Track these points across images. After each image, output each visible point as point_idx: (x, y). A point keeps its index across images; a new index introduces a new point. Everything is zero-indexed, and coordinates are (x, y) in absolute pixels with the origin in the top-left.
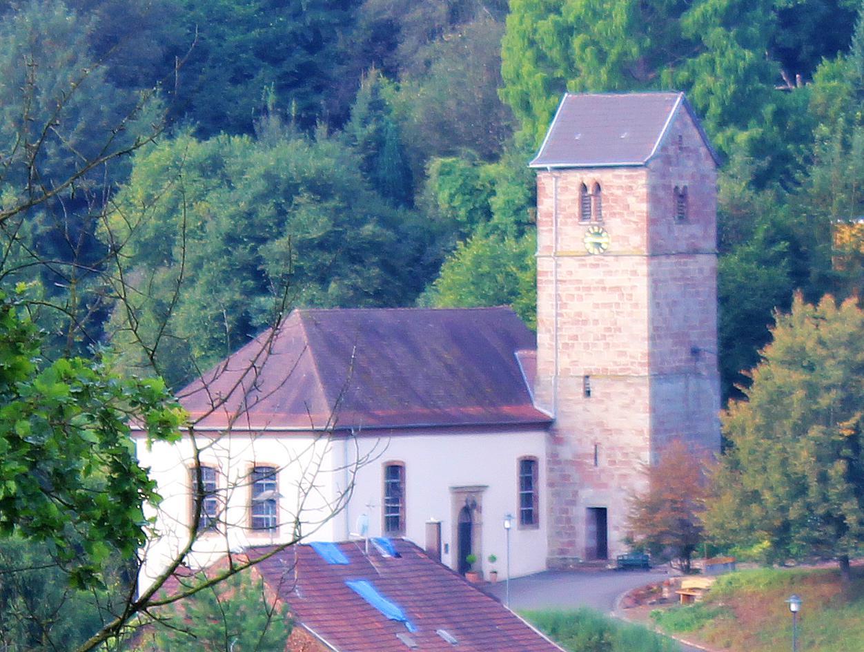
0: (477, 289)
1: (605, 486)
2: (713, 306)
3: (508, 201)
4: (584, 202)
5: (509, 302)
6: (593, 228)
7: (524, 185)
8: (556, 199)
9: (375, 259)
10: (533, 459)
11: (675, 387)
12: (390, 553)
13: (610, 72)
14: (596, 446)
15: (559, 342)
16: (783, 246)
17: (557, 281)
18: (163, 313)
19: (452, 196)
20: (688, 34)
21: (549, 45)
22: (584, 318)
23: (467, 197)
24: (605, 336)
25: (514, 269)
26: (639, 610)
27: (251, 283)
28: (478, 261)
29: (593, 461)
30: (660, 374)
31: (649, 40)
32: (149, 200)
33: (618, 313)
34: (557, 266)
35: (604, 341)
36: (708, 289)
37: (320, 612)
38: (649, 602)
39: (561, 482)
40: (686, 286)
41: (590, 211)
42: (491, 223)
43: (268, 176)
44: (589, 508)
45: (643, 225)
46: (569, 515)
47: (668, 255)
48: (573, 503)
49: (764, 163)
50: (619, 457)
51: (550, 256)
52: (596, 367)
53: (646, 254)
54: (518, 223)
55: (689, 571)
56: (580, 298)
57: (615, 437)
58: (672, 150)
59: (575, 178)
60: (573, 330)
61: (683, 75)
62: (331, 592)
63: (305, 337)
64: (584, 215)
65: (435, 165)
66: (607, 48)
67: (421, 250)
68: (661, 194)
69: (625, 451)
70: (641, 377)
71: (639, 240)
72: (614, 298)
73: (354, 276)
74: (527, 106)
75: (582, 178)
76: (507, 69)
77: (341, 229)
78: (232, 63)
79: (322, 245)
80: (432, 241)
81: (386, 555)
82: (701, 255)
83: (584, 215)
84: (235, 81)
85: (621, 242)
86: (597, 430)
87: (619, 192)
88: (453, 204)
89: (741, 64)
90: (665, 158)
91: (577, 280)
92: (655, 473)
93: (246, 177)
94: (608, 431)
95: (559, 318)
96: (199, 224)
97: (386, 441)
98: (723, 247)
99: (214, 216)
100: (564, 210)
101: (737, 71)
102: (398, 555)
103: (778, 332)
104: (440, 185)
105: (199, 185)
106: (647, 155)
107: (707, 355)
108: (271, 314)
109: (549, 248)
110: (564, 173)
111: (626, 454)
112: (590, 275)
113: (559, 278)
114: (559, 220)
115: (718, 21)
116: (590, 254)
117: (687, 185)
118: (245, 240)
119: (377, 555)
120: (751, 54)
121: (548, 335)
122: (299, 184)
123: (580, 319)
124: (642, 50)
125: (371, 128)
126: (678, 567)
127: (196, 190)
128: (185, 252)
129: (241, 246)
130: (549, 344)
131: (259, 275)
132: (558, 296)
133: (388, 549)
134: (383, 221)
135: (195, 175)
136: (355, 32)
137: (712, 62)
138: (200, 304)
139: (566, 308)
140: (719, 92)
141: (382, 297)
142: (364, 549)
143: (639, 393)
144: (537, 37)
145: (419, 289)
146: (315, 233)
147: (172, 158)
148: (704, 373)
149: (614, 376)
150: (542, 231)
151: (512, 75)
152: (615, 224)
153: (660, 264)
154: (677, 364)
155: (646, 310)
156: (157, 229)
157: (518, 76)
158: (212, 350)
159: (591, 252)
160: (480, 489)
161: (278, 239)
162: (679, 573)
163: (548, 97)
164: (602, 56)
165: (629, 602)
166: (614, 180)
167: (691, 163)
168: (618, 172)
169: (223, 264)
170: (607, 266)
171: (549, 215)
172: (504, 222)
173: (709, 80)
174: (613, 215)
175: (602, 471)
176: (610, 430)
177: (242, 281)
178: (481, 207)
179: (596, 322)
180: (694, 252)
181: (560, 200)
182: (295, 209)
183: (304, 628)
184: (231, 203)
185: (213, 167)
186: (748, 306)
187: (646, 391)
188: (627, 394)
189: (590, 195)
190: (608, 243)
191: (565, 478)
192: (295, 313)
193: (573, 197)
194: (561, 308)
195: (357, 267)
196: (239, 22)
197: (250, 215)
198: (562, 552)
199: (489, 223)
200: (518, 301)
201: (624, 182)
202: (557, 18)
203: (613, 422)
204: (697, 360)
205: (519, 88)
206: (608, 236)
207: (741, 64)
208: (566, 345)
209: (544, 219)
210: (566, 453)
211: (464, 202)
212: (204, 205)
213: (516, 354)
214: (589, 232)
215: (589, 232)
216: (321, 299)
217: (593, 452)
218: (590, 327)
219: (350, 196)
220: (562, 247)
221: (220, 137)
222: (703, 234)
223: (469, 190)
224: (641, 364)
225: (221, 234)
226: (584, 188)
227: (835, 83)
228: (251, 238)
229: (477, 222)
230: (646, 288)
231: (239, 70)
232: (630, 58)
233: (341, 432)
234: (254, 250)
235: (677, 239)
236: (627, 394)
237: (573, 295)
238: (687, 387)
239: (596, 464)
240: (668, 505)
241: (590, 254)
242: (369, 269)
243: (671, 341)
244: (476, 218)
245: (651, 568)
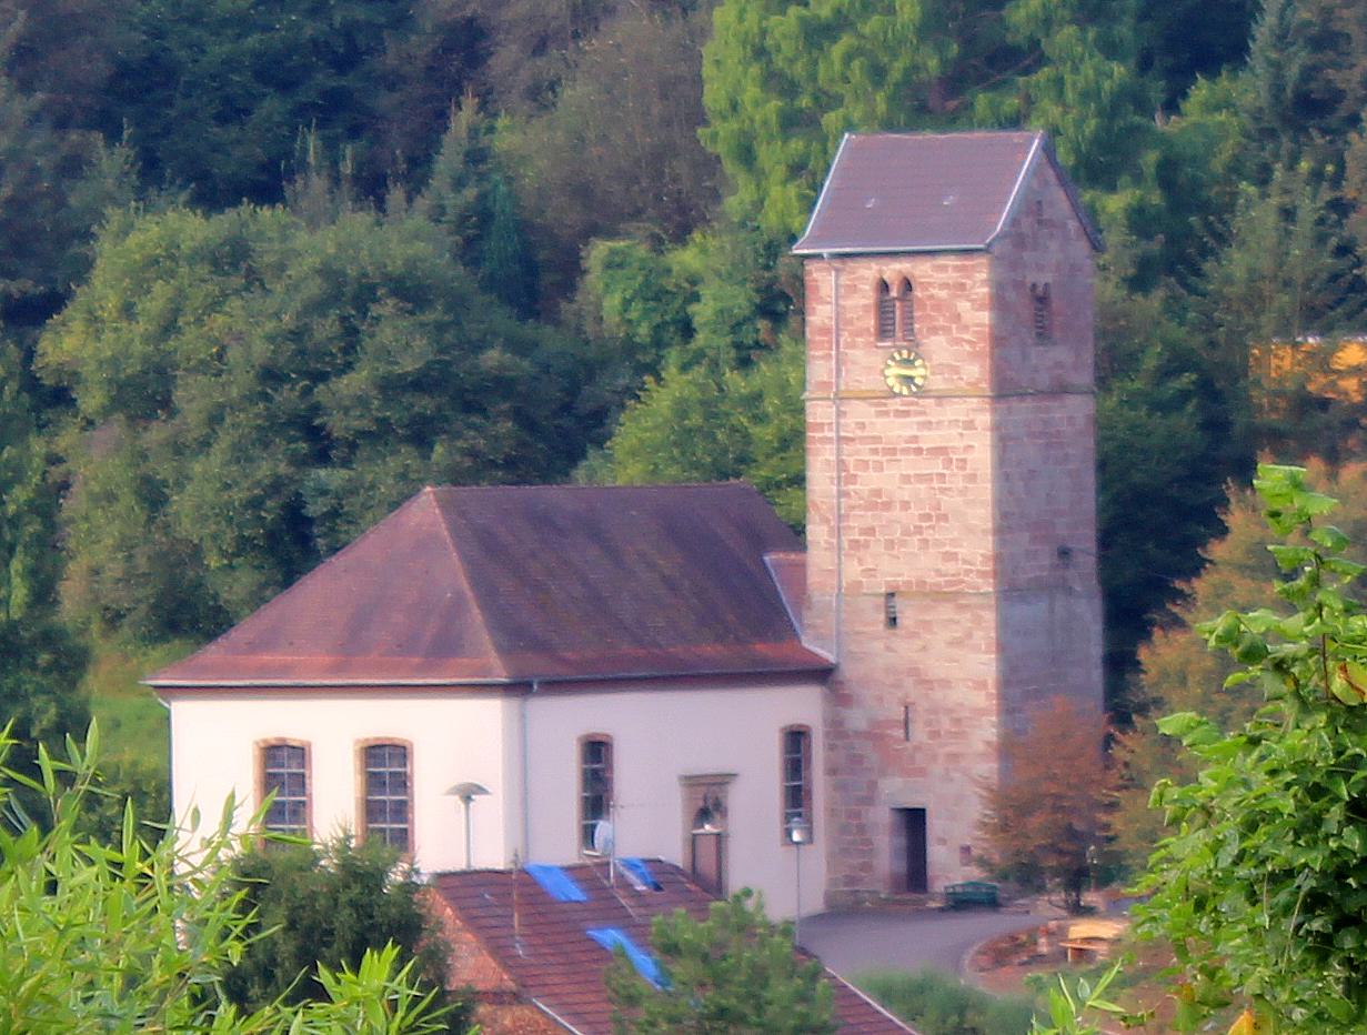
0: (683, 453)
1: (922, 772)
2: (1090, 479)
3: (722, 311)
4: (883, 310)
5: (738, 475)
6: (900, 354)
7: (748, 285)
8: (837, 305)
9: (505, 406)
10: (802, 729)
11: (1037, 610)
12: (646, 884)
13: (891, 99)
14: (906, 707)
15: (843, 538)
16: (1187, 379)
17: (840, 439)
18: (153, 496)
19: (627, 303)
20: (1017, 38)
21: (790, 55)
22: (884, 499)
23: (652, 304)
24: (921, 527)
25: (744, 420)
26: (1004, 973)
27: (303, 447)
28: (681, 410)
29: (902, 731)
30: (1012, 589)
31: (955, 46)
32: (128, 311)
33: (943, 491)
34: (840, 414)
35: (919, 537)
36: (1081, 454)
37: (556, 980)
38: (1017, 961)
39: (847, 767)
40: (1048, 446)
41: (894, 324)
42: (693, 346)
43: (326, 272)
44: (893, 809)
45: (984, 346)
46: (864, 821)
47: (1022, 396)
48: (869, 800)
49: (1155, 246)
50: (945, 724)
51: (829, 399)
52: (905, 578)
53: (990, 394)
54: (738, 346)
55: (1080, 911)
56: (879, 467)
57: (938, 694)
58: (1026, 225)
59: (869, 272)
60: (869, 519)
61: (1011, 103)
62: (568, 948)
63: (446, 533)
64: (884, 331)
65: (597, 252)
66: (886, 60)
67: (573, 391)
68: (1011, 296)
69: (955, 715)
70: (982, 594)
71: (976, 371)
72: (937, 466)
73: (472, 433)
74: (746, 156)
75: (880, 271)
76: (714, 96)
77: (447, 358)
78: (217, 89)
79: (420, 383)
80: (590, 377)
81: (641, 888)
82: (1071, 396)
83: (885, 331)
84: (222, 119)
85: (946, 376)
86: (909, 682)
87: (943, 294)
88: (627, 316)
89: (1107, 85)
90: (1017, 238)
91: (873, 437)
92: (1007, 749)
93: (288, 273)
94: (926, 683)
95: (842, 500)
96: (214, 350)
98: (1103, 383)
99: (239, 337)
100: (850, 322)
101: (1100, 97)
102: (658, 888)
103: (1236, 518)
104: (607, 285)
105: (210, 287)
106: (989, 233)
107: (1081, 559)
108: (337, 497)
109: (825, 385)
110: (851, 264)
111: (958, 721)
112: (897, 430)
113: (843, 434)
114: (842, 340)
115: (1067, 13)
116: (895, 395)
117: (1050, 281)
118: (293, 376)
119: (628, 886)
120: (1122, 69)
121: (826, 528)
122: (378, 284)
123: (879, 501)
124: (943, 62)
125: (470, 193)
126: (1062, 904)
127: (207, 296)
128: (193, 398)
129: (288, 387)
130: (826, 542)
131: (315, 433)
132: (841, 464)
133: (642, 876)
134: (521, 347)
135: (203, 270)
136: (414, 38)
137: (1059, 82)
138: (220, 481)
139: (855, 483)
140: (1071, 131)
141: (517, 468)
142: (608, 877)
143: (978, 620)
144: (769, 42)
145: (574, 456)
146: (409, 365)
147: (164, 244)
148: (1078, 588)
149: (938, 593)
150: (813, 357)
151: (723, 104)
152: (938, 347)
153: (1009, 409)
154: (1038, 573)
155: (989, 486)
156: (145, 359)
157: (735, 106)
158: (239, 556)
159: (896, 390)
160: (722, 780)
161: (346, 373)
162: (1064, 913)
163: (785, 141)
164: (878, 74)
165: (984, 961)
166: (935, 274)
167: (1054, 245)
168: (941, 261)
169: (257, 416)
170: (924, 413)
171: (825, 331)
172: (715, 345)
173: (1055, 111)
174: (934, 330)
175: (917, 748)
176: (927, 681)
177: (289, 443)
178: (675, 322)
179: (905, 505)
180: (1060, 390)
181: (844, 307)
182: (371, 325)
183: (538, 1008)
184: (270, 317)
185: (233, 259)
186: (1137, 477)
187: (990, 617)
188: (958, 622)
189: (894, 299)
190: (924, 377)
191: (856, 760)
192: (425, 494)
194: (846, 484)
195: (476, 419)
196: (225, 22)
197: (296, 335)
198: (851, 880)
199: (688, 347)
200: (752, 472)
201: (951, 276)
202: (803, 12)
203: (936, 667)
204: (1067, 566)
205: (735, 126)
206: (925, 367)
207: (1107, 85)
208: (855, 544)
209: (818, 338)
210: (856, 719)
211: (646, 313)
212: (220, 319)
213: (767, 558)
214: (893, 359)
215: (893, 359)
216: (419, 472)
217: (903, 717)
218: (897, 513)
219: (457, 303)
220: (847, 384)
221: (242, 208)
222: (1073, 359)
223: (654, 294)
224: (982, 574)
225: (253, 366)
226: (884, 287)
227: (1222, 117)
228: (304, 374)
229: (669, 345)
230: (989, 449)
231: (227, 100)
232: (923, 75)
233: (518, 688)
234: (307, 392)
235: (1036, 370)
236: (958, 622)
237: (867, 462)
238: (1052, 611)
239: (907, 738)
240: (1049, 802)
241: (895, 395)
242: (495, 423)
243: (1026, 536)
244: (666, 337)
245: (1001, 905)
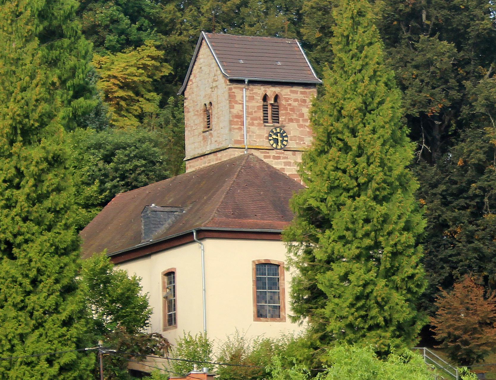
97: (154, 258)
168: (295, 89)
170: (287, 158)
174: (291, 120)
193: (258, 104)
201: (300, 96)
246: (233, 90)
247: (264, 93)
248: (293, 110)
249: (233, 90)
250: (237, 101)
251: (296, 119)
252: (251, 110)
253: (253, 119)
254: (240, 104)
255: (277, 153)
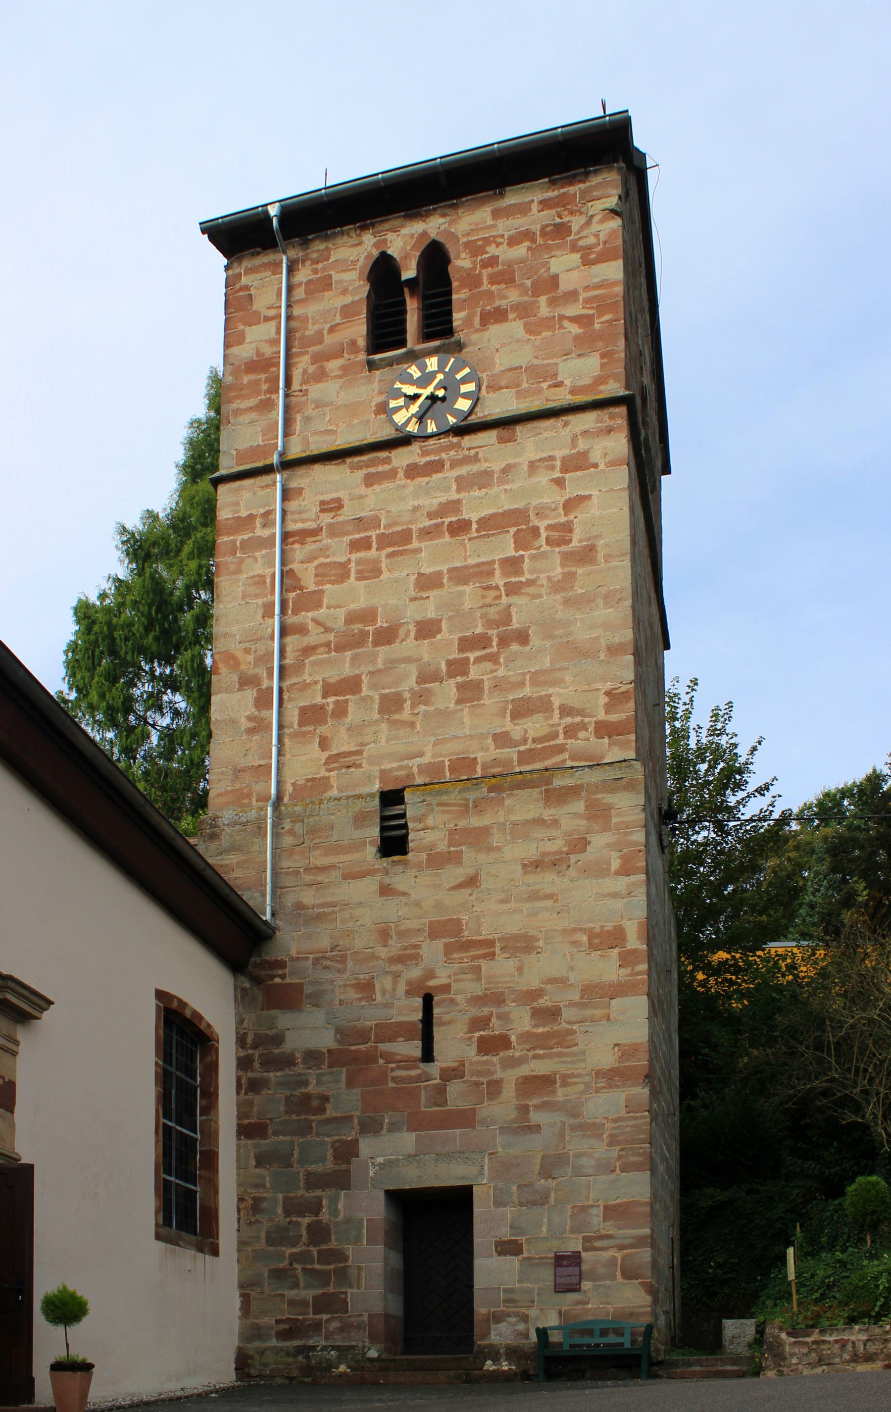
246: (244, 280)
247: (376, 253)
248: (506, 277)
249: (244, 280)
250: (258, 313)
251: (516, 307)
252: (317, 327)
253: (318, 358)
254: (267, 319)
255: (425, 453)
